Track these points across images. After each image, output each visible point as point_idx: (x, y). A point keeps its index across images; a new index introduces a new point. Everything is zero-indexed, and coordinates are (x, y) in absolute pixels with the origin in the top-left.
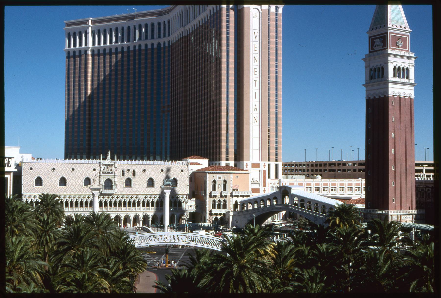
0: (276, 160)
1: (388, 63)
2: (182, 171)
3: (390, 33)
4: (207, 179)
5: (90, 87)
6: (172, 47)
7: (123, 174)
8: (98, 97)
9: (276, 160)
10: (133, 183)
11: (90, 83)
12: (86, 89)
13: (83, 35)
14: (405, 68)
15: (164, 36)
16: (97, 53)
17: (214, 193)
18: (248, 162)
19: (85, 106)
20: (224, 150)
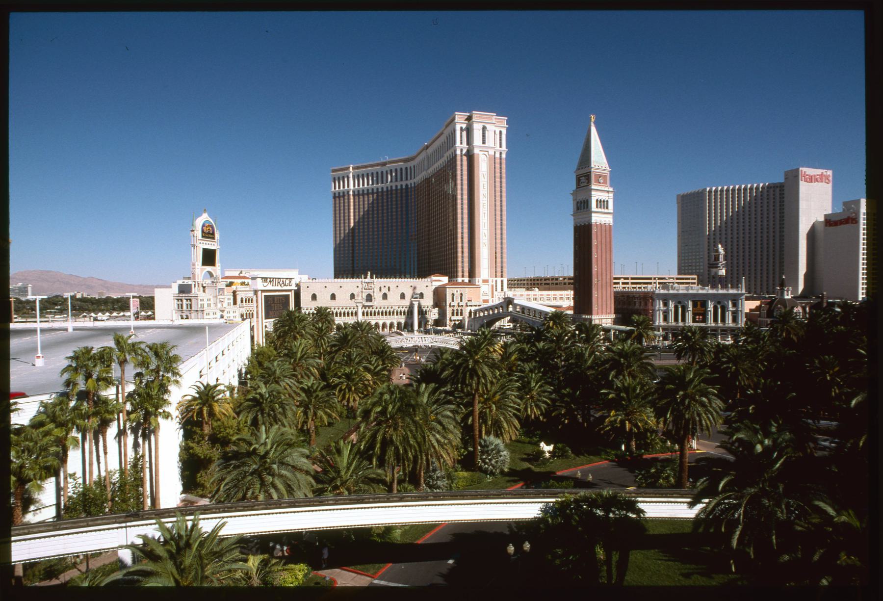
2: (427, 286)
4: (447, 293)
5: (352, 221)
6: (417, 188)
7: (380, 291)
8: (359, 229)
9: (502, 277)
10: (388, 296)
11: (352, 218)
12: (349, 223)
13: (346, 179)
15: (411, 179)
19: (349, 236)
20: (460, 269)
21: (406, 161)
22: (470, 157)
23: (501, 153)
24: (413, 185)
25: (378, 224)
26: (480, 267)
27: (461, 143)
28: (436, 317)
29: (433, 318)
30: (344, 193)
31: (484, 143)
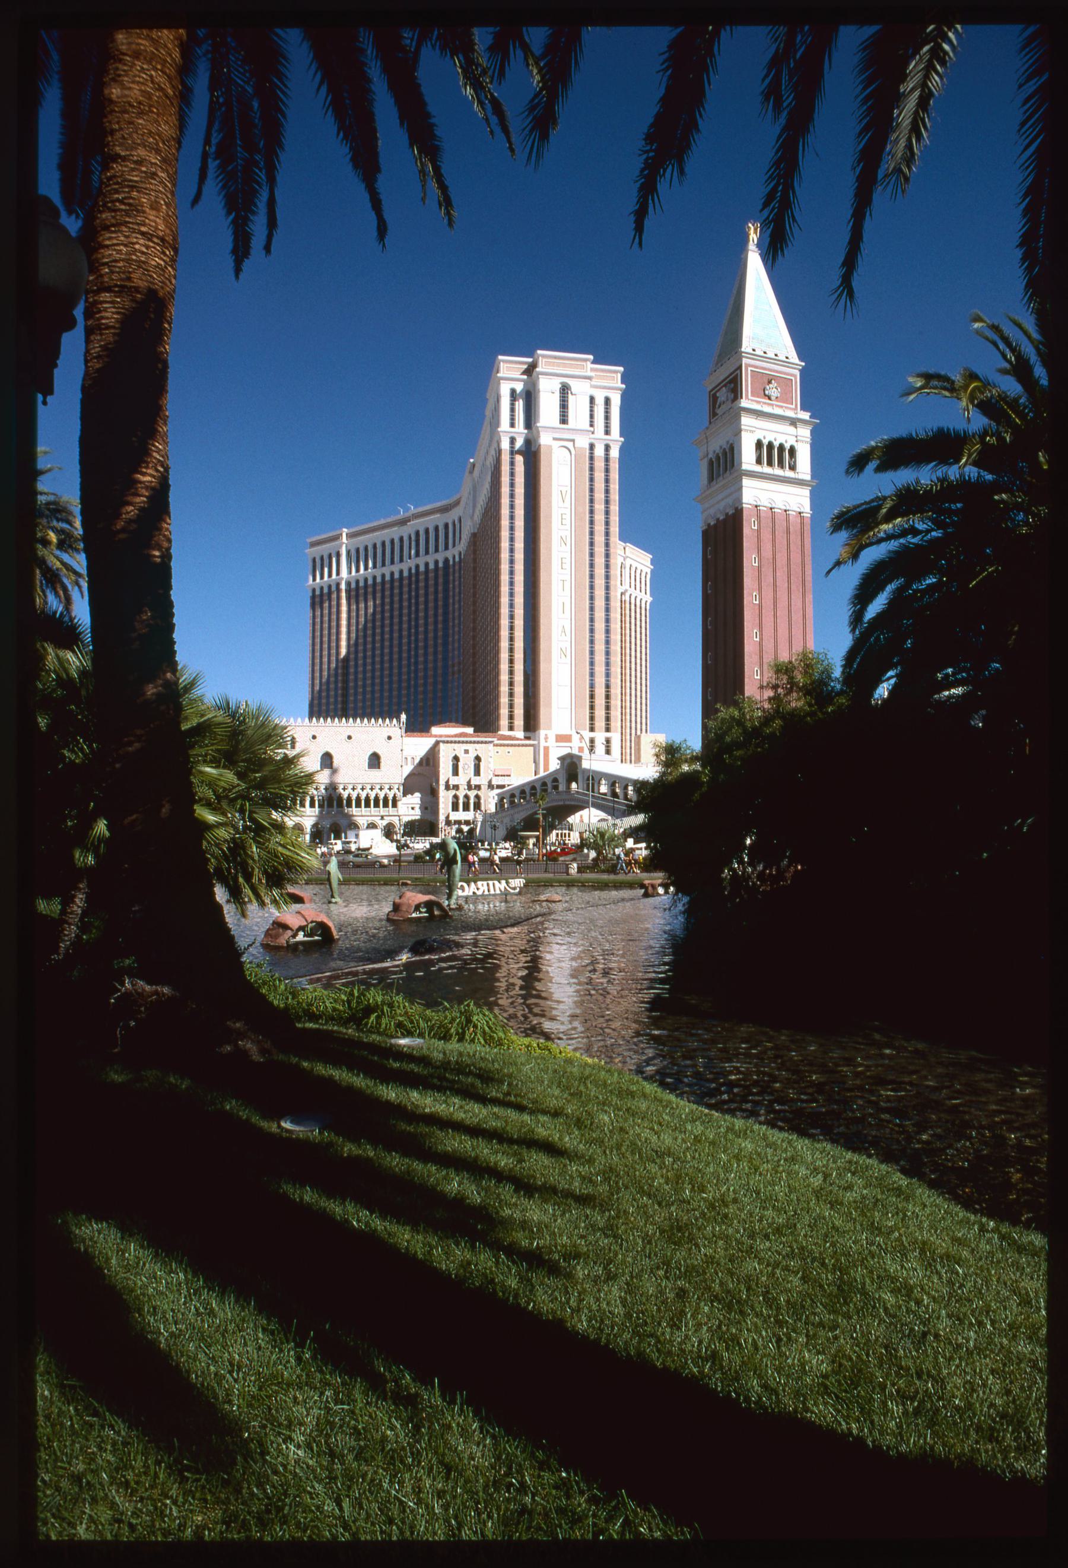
0: (608, 730)
1: (740, 431)
2: (389, 738)
3: (747, 366)
5: (344, 643)
8: (356, 659)
9: (608, 730)
12: (338, 647)
13: (334, 560)
14: (787, 446)
16: (357, 592)
17: (454, 781)
18: (547, 732)
19: (336, 675)
20: (504, 712)
21: (445, 510)
22: (531, 454)
23: (607, 448)
24: (457, 559)
25: (426, 654)
26: (549, 705)
27: (512, 425)
28: (416, 815)
29: (406, 819)
30: (330, 587)
31: (564, 420)
